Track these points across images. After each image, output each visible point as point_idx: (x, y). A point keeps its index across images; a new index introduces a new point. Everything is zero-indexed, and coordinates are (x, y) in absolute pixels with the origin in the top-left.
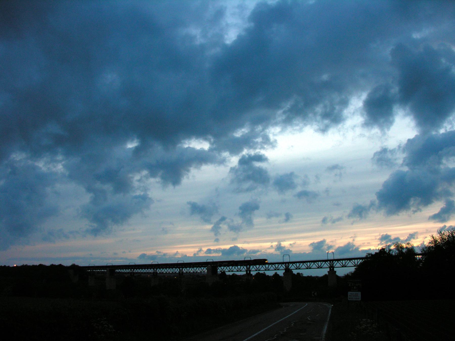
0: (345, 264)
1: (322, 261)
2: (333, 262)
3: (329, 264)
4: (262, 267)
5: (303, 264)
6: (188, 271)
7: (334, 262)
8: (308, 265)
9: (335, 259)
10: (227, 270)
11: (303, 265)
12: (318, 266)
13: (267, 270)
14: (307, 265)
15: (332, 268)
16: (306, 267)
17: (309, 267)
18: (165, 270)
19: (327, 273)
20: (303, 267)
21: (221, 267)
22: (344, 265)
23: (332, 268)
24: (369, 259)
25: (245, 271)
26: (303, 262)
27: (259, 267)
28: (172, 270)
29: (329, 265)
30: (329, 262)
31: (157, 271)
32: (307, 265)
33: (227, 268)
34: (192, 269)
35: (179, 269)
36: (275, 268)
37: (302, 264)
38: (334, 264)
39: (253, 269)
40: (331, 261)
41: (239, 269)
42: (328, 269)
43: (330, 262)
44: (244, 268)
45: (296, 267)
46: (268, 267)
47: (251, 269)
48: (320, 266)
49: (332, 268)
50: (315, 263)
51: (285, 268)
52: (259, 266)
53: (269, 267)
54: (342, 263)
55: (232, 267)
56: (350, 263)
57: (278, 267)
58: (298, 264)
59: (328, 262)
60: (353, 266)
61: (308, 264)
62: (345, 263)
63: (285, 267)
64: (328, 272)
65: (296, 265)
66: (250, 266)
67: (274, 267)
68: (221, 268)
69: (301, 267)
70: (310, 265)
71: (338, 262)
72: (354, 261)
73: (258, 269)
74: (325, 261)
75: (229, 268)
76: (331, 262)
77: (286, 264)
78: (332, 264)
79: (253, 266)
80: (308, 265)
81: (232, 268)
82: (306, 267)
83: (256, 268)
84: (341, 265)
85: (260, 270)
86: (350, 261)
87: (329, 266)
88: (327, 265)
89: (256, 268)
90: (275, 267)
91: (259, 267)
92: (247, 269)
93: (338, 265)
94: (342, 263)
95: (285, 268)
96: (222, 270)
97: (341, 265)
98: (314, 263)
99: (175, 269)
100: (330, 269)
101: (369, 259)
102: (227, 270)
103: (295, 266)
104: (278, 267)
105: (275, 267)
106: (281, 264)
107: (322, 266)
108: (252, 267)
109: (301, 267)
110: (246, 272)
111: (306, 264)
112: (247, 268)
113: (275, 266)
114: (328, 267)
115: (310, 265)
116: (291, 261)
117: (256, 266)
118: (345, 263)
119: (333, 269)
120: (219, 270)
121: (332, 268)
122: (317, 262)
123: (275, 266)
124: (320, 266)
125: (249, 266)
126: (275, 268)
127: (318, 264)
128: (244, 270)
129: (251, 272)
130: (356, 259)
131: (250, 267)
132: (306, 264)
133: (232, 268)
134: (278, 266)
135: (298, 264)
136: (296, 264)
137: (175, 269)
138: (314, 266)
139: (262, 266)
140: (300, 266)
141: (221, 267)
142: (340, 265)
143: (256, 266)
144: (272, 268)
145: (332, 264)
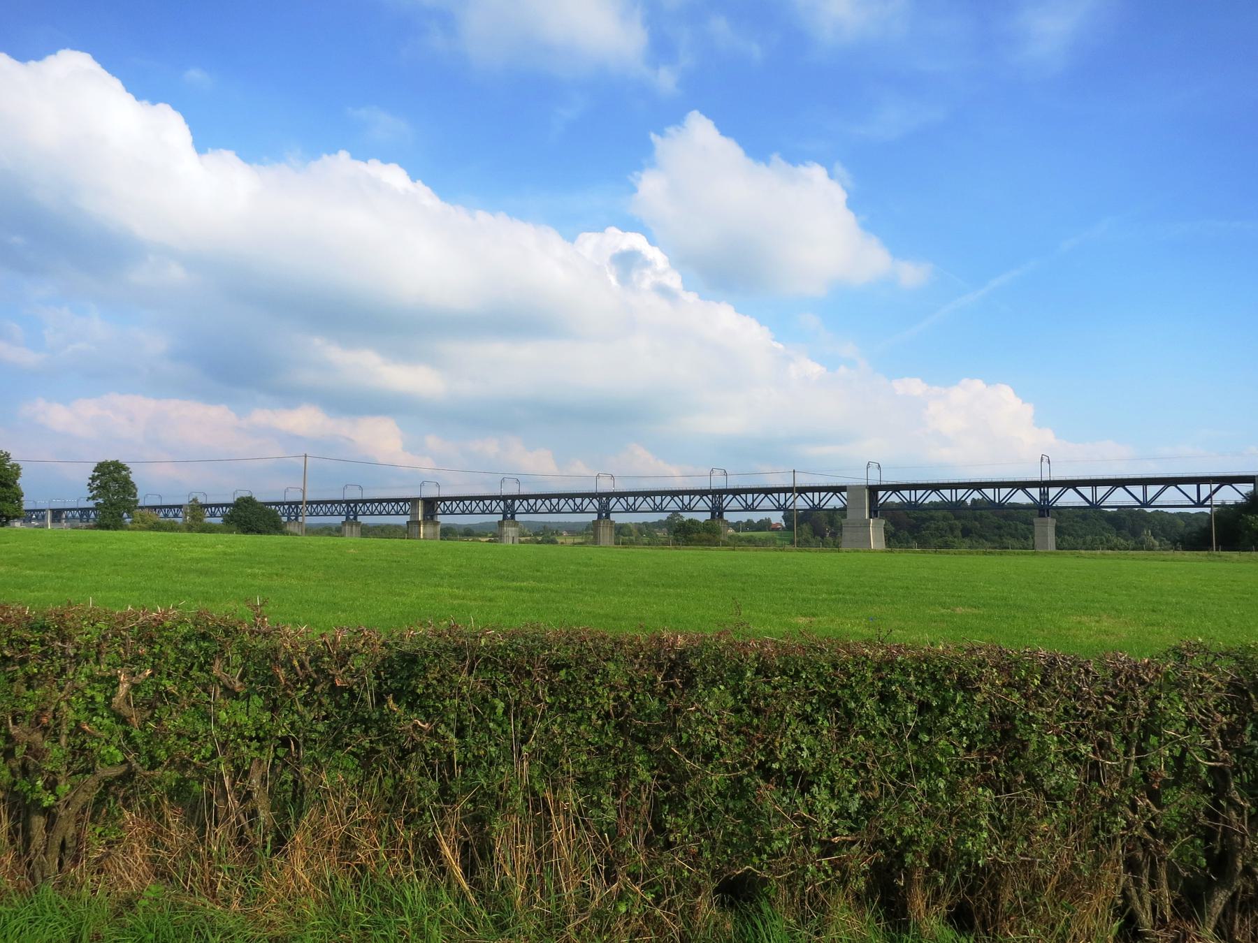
2: (297, 507)
3: (712, 502)
7: (724, 496)
8: (686, 502)
9: (732, 487)
13: (532, 511)
14: (682, 501)
18: (395, 508)
20: (645, 506)
22: (749, 506)
26: (647, 494)
27: (582, 504)
28: (309, 509)
30: (710, 496)
31: (358, 509)
32: (682, 501)
37: (669, 498)
38: (723, 501)
39: (618, 507)
44: (1035, 492)
48: (686, 507)
50: (676, 498)
52: (583, 501)
54: (746, 502)
56: (219, 512)
57: (634, 503)
61: (686, 498)
62: (754, 501)
65: (654, 501)
68: (528, 504)
70: (662, 501)
72: (776, 495)
74: (702, 493)
75: (551, 504)
77: (290, 506)
80: (686, 502)
81: (535, 503)
83: (575, 504)
86: (766, 496)
87: (1193, 501)
88: (703, 504)
89: (575, 504)
91: (582, 504)
92: (507, 506)
93: (735, 504)
94: (746, 502)
96: (467, 508)
98: (701, 498)
100: (600, 516)
102: (543, 507)
104: (634, 503)
105: (628, 504)
107: (755, 504)
113: (627, 501)
115: (662, 501)
117: (574, 501)
118: (754, 501)
123: (627, 501)
124: (686, 507)
128: (701, 505)
129: (725, 514)
133: (535, 503)
134: (635, 500)
138: (645, 506)
139: (567, 502)
140: (664, 504)
142: (1083, 500)
143: (574, 501)
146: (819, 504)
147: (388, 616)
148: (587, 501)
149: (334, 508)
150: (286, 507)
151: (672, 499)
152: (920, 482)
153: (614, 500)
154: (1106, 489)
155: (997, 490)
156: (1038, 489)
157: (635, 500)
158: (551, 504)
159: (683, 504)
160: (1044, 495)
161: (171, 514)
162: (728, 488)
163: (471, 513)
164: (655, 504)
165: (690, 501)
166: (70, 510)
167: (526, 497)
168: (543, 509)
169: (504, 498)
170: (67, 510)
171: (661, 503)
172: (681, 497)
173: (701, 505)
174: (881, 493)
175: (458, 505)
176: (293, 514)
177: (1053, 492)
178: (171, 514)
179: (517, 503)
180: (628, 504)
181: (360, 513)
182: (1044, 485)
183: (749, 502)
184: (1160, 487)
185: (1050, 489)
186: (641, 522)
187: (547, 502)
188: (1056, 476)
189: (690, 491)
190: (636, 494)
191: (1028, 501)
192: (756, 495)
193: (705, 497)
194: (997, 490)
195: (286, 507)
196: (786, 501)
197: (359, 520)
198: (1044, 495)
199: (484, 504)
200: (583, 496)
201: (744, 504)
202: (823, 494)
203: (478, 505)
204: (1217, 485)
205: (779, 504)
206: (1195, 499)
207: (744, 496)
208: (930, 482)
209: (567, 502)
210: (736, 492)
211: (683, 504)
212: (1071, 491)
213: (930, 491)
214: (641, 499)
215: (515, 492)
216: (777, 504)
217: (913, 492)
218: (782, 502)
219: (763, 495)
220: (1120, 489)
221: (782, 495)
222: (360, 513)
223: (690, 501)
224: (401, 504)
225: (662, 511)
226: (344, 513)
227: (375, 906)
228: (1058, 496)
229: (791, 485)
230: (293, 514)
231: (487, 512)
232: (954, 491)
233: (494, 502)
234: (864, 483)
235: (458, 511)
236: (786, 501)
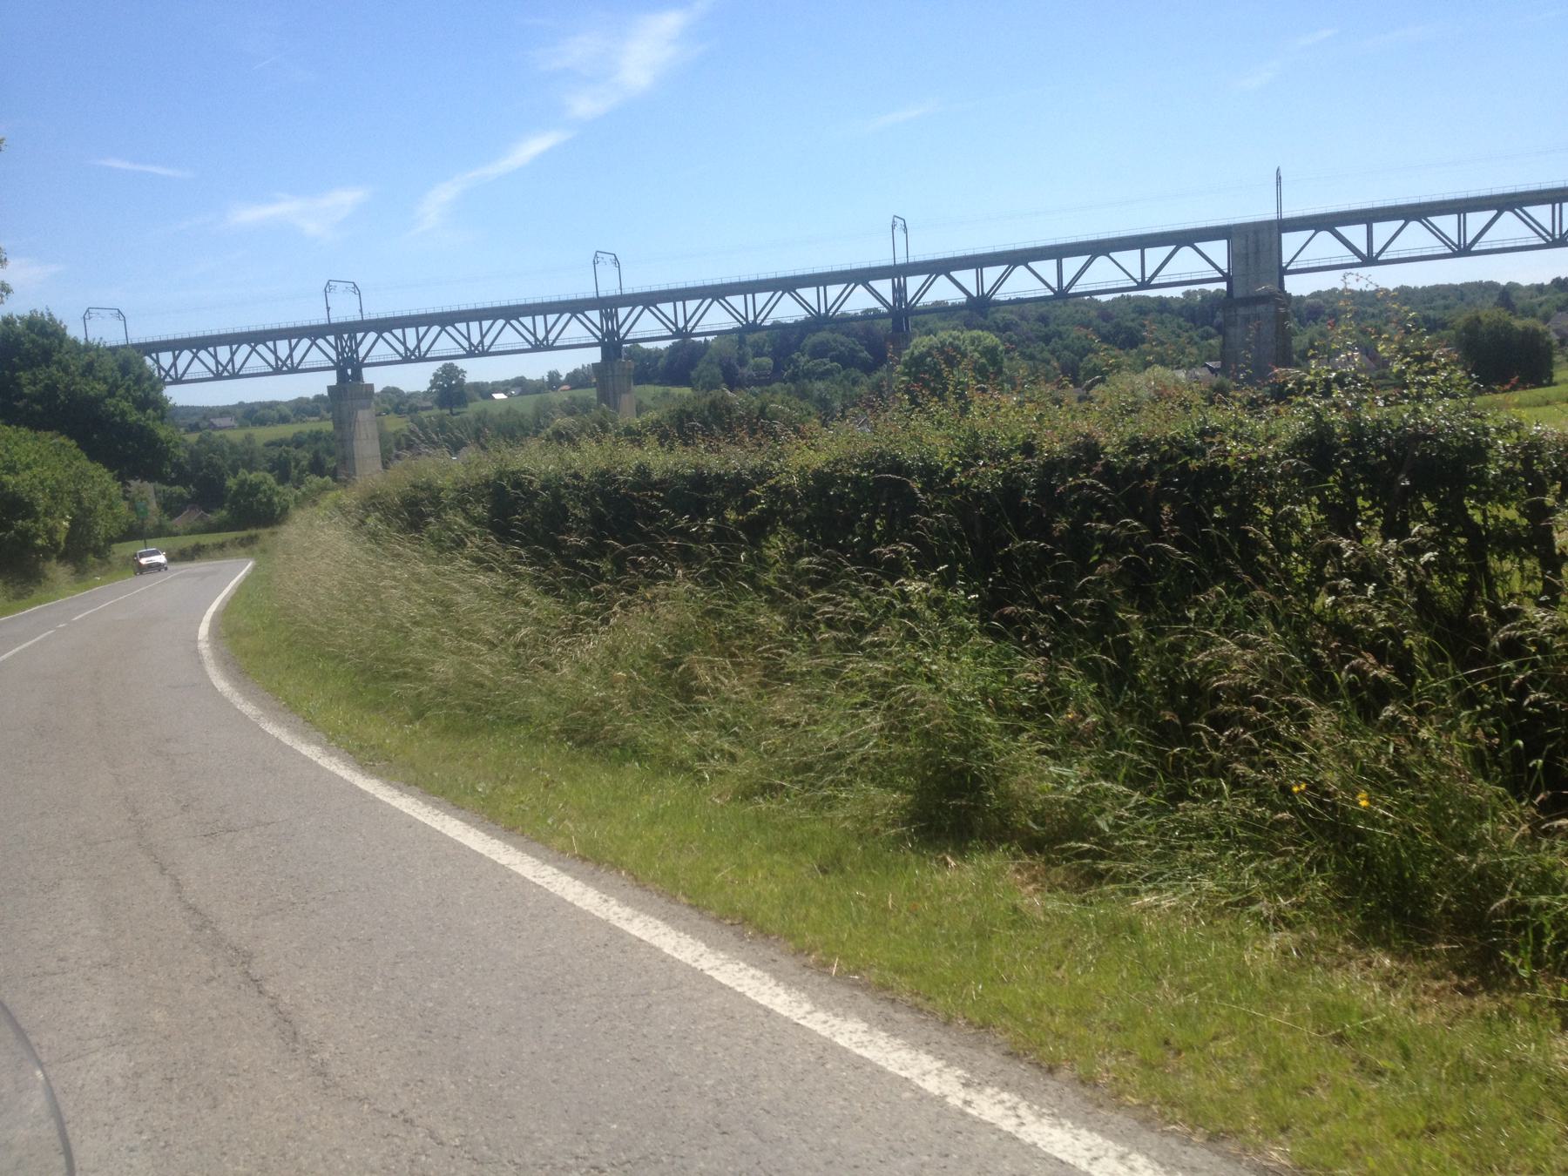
0: (418, 347)
1: (487, 318)
2: (352, 337)
3: (336, 348)
5: (195, 356)
7: (359, 336)
9: (374, 317)
11: (380, 340)
12: (214, 369)
15: (349, 371)
16: (273, 362)
17: (172, 372)
19: (378, 389)
20: (255, 363)
22: (541, 343)
23: (349, 371)
29: (333, 355)
37: (306, 342)
38: (358, 345)
40: (345, 331)
42: (331, 378)
43: (339, 337)
44: (884, 287)
45: (214, 369)
49: (349, 368)
50: (261, 348)
54: (404, 344)
57: (231, 360)
59: (329, 338)
60: (527, 346)
62: (420, 341)
63: (334, 357)
64: (330, 388)
69: (185, 372)
71: (380, 336)
72: (462, 326)
74: (314, 333)
76: (346, 336)
78: (351, 347)
82: (273, 362)
84: (330, 359)
85: (1153, 282)
86: (443, 329)
88: (320, 354)
91: (174, 365)
93: (382, 351)
94: (404, 344)
97: (330, 359)
98: (314, 343)
100: (342, 377)
103: (211, 363)
104: (231, 360)
105: (218, 362)
108: (249, 349)
109: (185, 372)
110: (334, 373)
111: (272, 347)
113: (215, 357)
114: (1065, 283)
116: (628, 290)
118: (420, 341)
119: (358, 376)
121: (349, 368)
122: (461, 321)
123: (215, 357)
124: (284, 363)
127: (275, 352)
128: (315, 357)
129: (365, 371)
130: (281, 338)
132: (272, 347)
134: (233, 354)
136: (270, 344)
138: (255, 363)
140: (297, 356)
142: (1044, 286)
145: (351, 347)
146: (481, 342)
147: (777, 857)
148: (186, 356)
151: (253, 349)
152: (691, 285)
154: (1390, 227)
155: (821, 288)
157: (233, 354)
159: (277, 358)
160: (899, 291)
162: (911, 260)
164: (218, 362)
165: (292, 350)
172: (211, 349)
173: (315, 357)
174: (623, 312)
177: (913, 283)
182: (898, 272)
183: (412, 344)
184: (1167, 250)
186: (1547, 282)
188: (919, 254)
189: (175, 341)
190: (234, 340)
191: (960, 298)
192: (422, 330)
193: (320, 342)
194: (821, 288)
196: (483, 336)
198: (899, 291)
200: (293, 333)
201: (401, 349)
202: (551, 318)
205: (407, 349)
206: (1138, 276)
207: (398, 332)
208: (708, 283)
210: (382, 326)
211: (277, 358)
212: (1325, 236)
213: (640, 308)
214: (245, 349)
216: (402, 350)
217: (679, 304)
218: (475, 339)
219: (501, 322)
220: (1414, 226)
221: (474, 326)
223: (292, 350)
228: (842, 298)
229: (591, 294)
232: (749, 297)
236: (483, 336)
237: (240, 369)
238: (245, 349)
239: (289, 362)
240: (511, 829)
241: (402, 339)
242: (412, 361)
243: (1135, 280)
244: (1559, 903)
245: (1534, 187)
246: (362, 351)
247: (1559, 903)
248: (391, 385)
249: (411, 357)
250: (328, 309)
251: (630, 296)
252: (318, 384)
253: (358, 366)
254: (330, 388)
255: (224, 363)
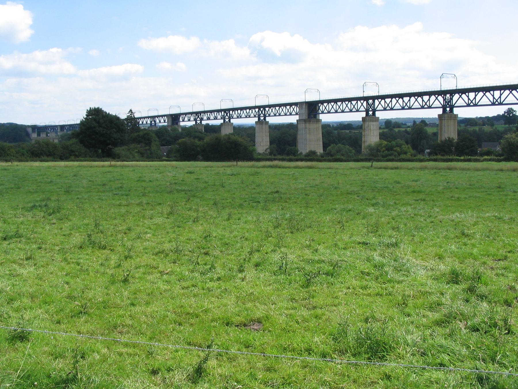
4: (362, 106)
6: (354, 107)
10: (348, 109)
17: (474, 102)
18: (334, 107)
20: (485, 101)
21: (403, 99)
24: (91, 117)
25: (194, 121)
26: (486, 90)
33: (397, 101)
34: (362, 104)
35: (365, 102)
36: (467, 102)
37: (507, 92)
39: (461, 102)
41: (426, 104)
42: (440, 111)
46: (475, 98)
47: (454, 103)
51: (442, 103)
53: (502, 96)
55: (410, 98)
58: (499, 92)
64: (439, 115)
65: (493, 96)
66: (453, 96)
67: (466, 99)
70: (501, 95)
73: (472, 102)
75: (423, 100)
77: (259, 109)
79: (437, 96)
81: (429, 100)
85: (432, 106)
88: (439, 101)
90: (492, 97)
93: (461, 102)
95: (442, 103)
96: (388, 105)
99: (290, 107)
100: (444, 111)
101: (91, 117)
103: (491, 98)
105: (469, 99)
106: (483, 92)
108: (483, 94)
110: (442, 109)
112: (444, 100)
113: (468, 97)
115: (501, 95)
117: (422, 98)
119: (451, 111)
120: (355, 108)
123: (468, 97)
125: (450, 96)
126: (467, 102)
129: (455, 109)
131: (452, 99)
133: (429, 100)
134: (476, 96)
135: (497, 93)
137: (290, 107)
138: (485, 101)
139: (437, 98)
141: (403, 99)
143: (422, 98)
144: (398, 106)
149: (292, 109)
150: (257, 110)
151: (511, 92)
153: (456, 96)
156: (474, 93)
157: (476, 96)
158: (423, 100)
161: (212, 117)
163: (392, 109)
166: (144, 118)
167: (383, 97)
168: (416, 105)
169: (366, 99)
170: (183, 114)
171: (500, 97)
172: (492, 92)
175: (380, 103)
176: (262, 115)
178: (212, 117)
179: (377, 102)
180: (469, 99)
181: (267, 115)
185: (470, 93)
187: (420, 99)
190: (476, 90)
195: (257, 110)
197: (267, 120)
199: (385, 102)
200: (430, 94)
203: (362, 104)
204: (503, 91)
209: (437, 98)
215: (452, 87)
222: (267, 115)
224: (339, 103)
225: (501, 104)
226: (257, 116)
227: (447, 235)
230: (262, 115)
231: (388, 108)
233: (359, 102)
234: (169, 114)
235: (333, 111)
237: (432, 105)
238: (481, 94)
239: (499, 100)
240: (85, 157)
241: (492, 94)
242: (472, 106)
243: (491, 102)
244: (517, 329)
245: (495, 85)
246: (454, 101)
247: (517, 329)
248: (486, 116)
249: (216, 118)
250: (364, 92)
251: (459, 90)
252: (434, 114)
253: (452, 107)
254: (439, 115)
255: (472, 100)
